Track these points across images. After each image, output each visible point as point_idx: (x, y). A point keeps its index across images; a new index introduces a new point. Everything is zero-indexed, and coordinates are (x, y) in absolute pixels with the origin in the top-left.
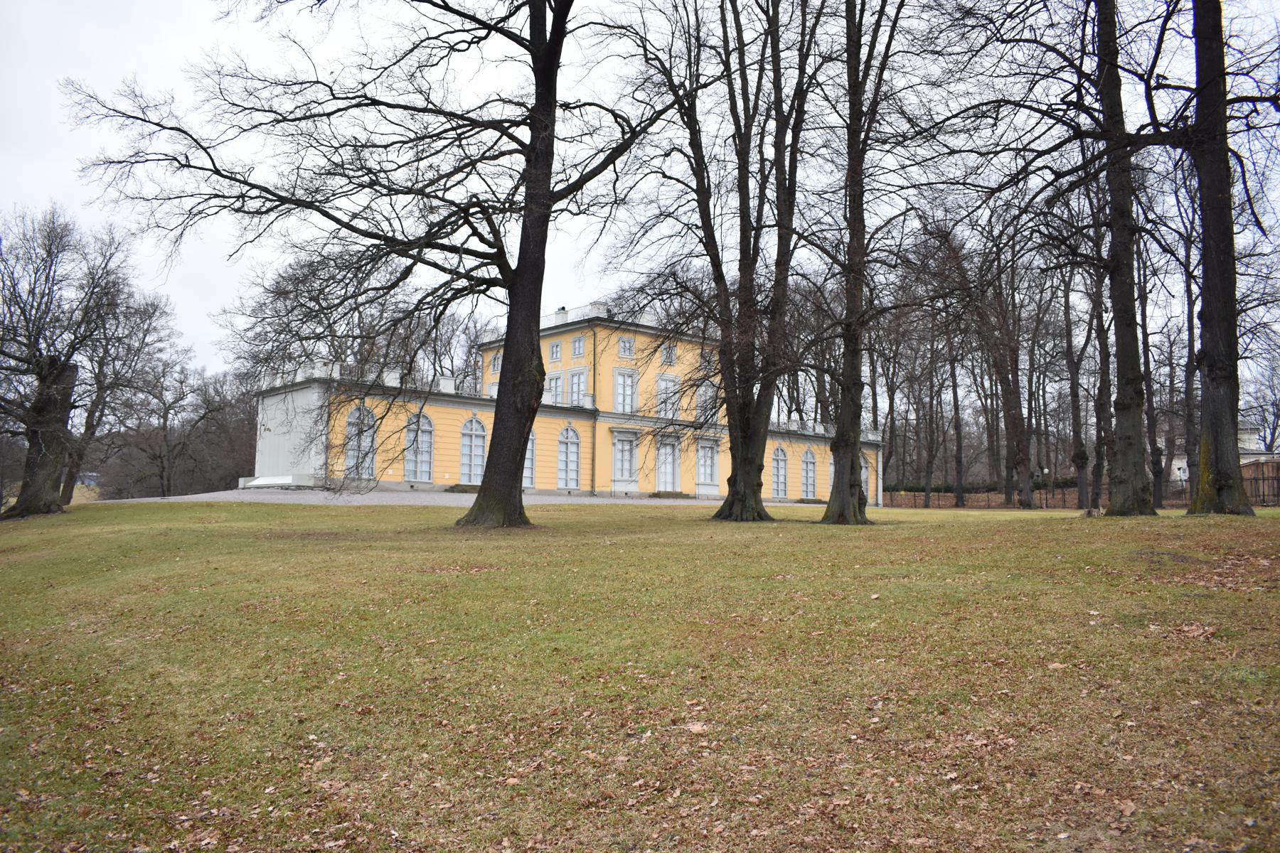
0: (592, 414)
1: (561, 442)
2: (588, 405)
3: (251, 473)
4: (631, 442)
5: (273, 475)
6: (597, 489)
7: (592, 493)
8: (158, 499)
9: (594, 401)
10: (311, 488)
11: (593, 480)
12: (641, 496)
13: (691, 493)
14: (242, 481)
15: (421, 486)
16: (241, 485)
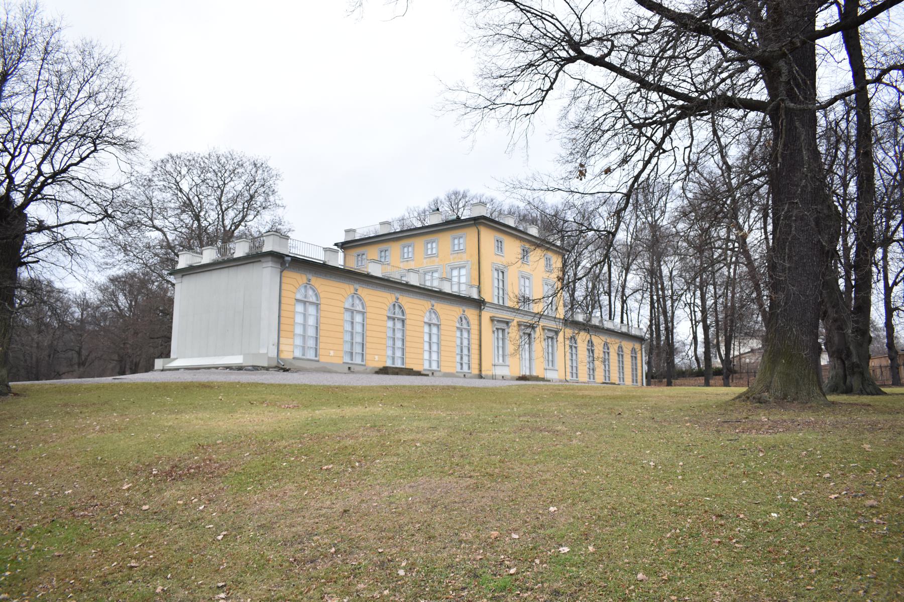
0: (479, 304)
1: (389, 318)
2: (475, 296)
3: (166, 353)
4: (503, 330)
5: (200, 355)
6: (483, 373)
7: (480, 377)
8: (108, 380)
9: (479, 292)
10: (267, 369)
11: (480, 365)
12: (512, 379)
13: (541, 376)
14: (159, 363)
15: (357, 368)
16: (156, 367)
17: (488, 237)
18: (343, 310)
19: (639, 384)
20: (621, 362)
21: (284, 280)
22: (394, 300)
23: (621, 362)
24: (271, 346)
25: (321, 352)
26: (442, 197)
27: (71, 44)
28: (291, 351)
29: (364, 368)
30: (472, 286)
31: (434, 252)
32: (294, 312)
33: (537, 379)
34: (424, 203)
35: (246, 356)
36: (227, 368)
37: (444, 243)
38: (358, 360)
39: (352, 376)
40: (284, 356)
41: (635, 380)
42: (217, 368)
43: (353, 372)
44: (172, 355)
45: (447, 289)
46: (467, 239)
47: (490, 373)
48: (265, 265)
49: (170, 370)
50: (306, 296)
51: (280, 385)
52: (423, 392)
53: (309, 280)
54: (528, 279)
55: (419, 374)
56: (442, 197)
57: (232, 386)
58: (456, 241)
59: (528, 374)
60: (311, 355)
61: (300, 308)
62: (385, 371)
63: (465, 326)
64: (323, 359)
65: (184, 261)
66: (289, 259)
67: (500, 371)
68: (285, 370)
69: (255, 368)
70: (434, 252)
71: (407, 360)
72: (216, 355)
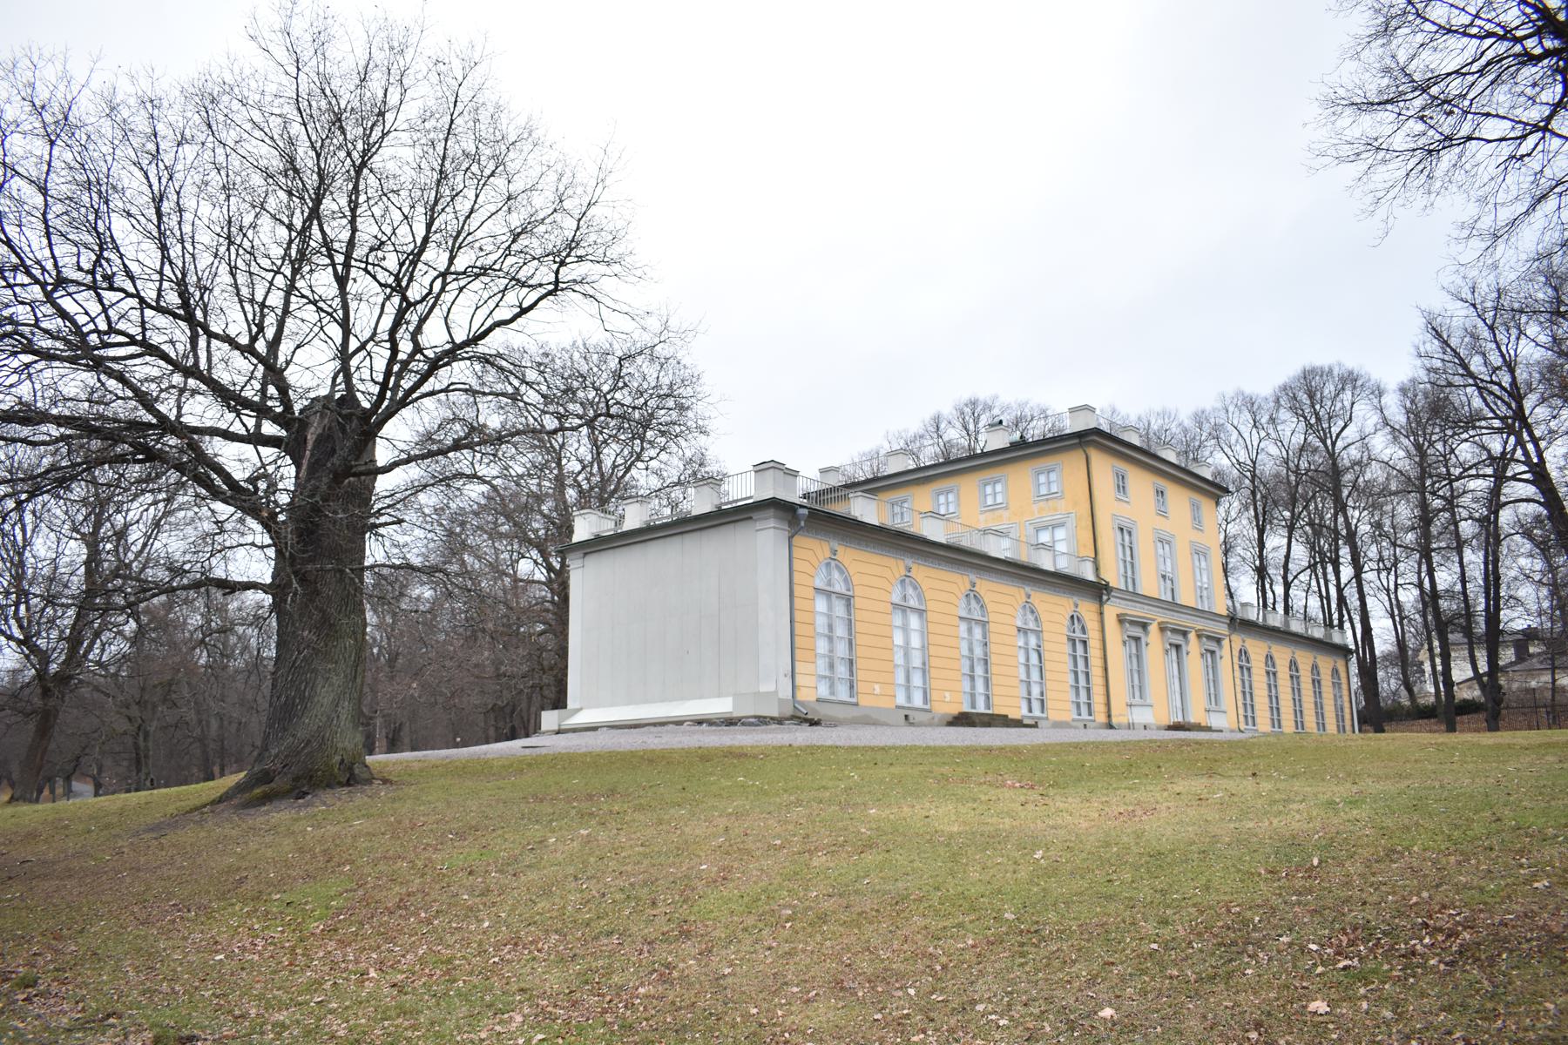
0: (1098, 591)
2: (1091, 577)
3: (559, 701)
5: (630, 701)
6: (1115, 721)
7: (1111, 726)
9: (1097, 569)
10: (779, 721)
12: (1159, 728)
14: (549, 719)
16: (543, 728)
17: (1104, 467)
18: (890, 607)
19: (1348, 728)
20: (1318, 694)
21: (797, 553)
22: (968, 587)
23: (1318, 694)
24: (781, 677)
25: (861, 687)
26: (948, 410)
27: (494, 98)
28: (813, 690)
29: (929, 716)
30: (1083, 559)
31: (999, 500)
32: (813, 612)
33: (1198, 727)
34: (913, 422)
35: (736, 696)
36: (700, 722)
37: (1020, 481)
38: (918, 701)
39: (909, 730)
40: (803, 695)
41: (1341, 728)
42: (679, 723)
43: (912, 724)
44: (571, 704)
45: (1047, 564)
46: (1066, 472)
47: (1124, 720)
48: (759, 525)
49: (574, 730)
50: (829, 583)
51: (883, 749)
52: (1211, 743)
53: (835, 553)
54: (1169, 543)
55: (1018, 723)
56: (948, 410)
57: (705, 756)
58: (989, 489)
59: (1180, 719)
60: (843, 694)
61: (821, 605)
62: (963, 720)
63: (1078, 634)
64: (864, 701)
65: (584, 528)
66: (806, 511)
67: (1142, 716)
68: (814, 723)
69: (762, 721)
70: (999, 500)
71: (995, 700)
72: (664, 699)
